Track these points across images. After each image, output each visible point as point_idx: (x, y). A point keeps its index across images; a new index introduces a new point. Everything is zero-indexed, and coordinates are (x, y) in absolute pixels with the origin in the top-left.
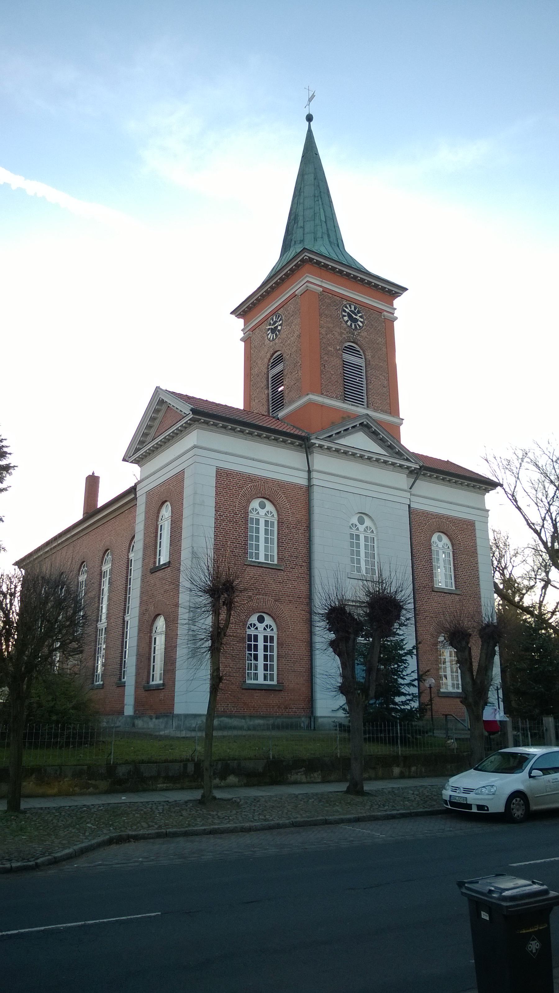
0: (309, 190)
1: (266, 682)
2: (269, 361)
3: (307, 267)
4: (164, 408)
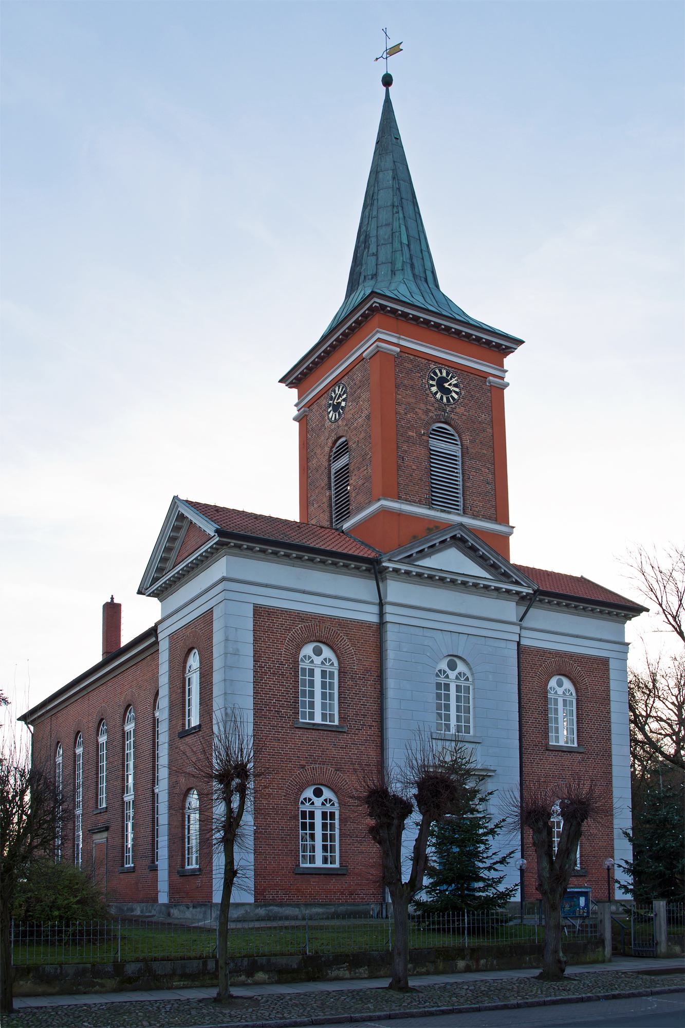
0: (385, 197)
2: (331, 451)
3: (377, 319)
4: (185, 525)
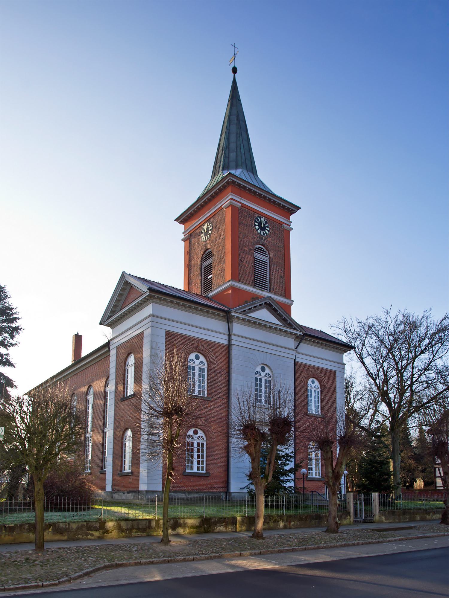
1: (198, 472)
2: (202, 256)
3: (229, 189)
4: (128, 288)
